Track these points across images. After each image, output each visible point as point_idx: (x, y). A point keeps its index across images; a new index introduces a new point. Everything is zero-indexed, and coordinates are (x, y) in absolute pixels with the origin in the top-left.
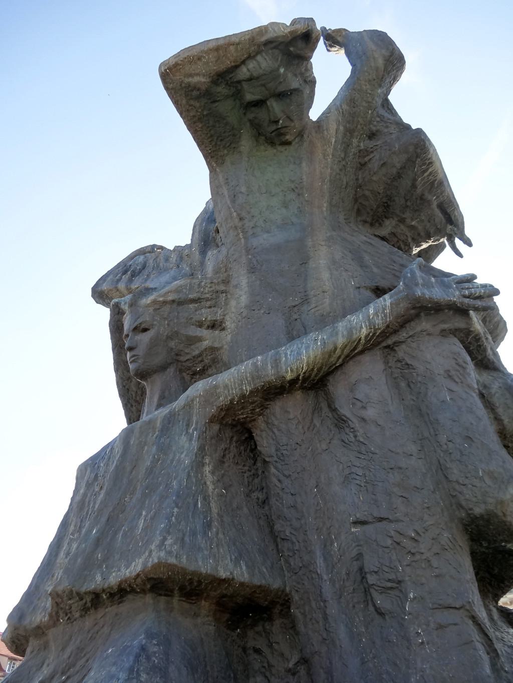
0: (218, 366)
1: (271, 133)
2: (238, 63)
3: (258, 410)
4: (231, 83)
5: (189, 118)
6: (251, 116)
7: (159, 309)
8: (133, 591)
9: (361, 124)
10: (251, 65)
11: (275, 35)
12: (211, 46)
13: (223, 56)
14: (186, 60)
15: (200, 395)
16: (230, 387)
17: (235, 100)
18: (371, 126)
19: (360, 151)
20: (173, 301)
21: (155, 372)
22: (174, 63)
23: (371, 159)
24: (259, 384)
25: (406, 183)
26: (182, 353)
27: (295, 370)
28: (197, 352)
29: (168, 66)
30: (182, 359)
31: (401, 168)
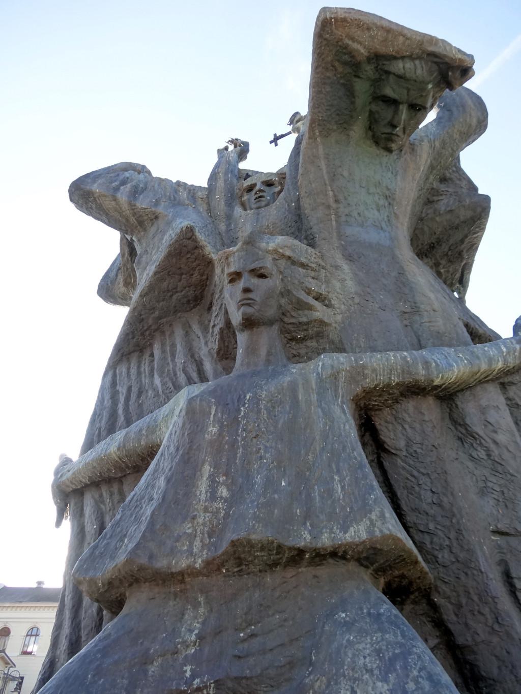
0: (321, 341)
1: (382, 134)
2: (398, 56)
3: (390, 402)
4: (380, 69)
5: (322, 76)
6: (374, 107)
7: (277, 260)
8: (344, 557)
9: (441, 166)
10: (409, 65)
11: (445, 53)
12: (385, 24)
13: (391, 41)
14: (356, 22)
15: (346, 369)
16: (378, 372)
17: (371, 85)
18: (446, 172)
19: (432, 189)
20: (289, 258)
21: (264, 324)
22: (342, 16)
23: (439, 200)
24: (408, 379)
25: (458, 236)
26: (288, 314)
27: (445, 378)
28: (304, 320)
29: (336, 15)
30: (286, 319)
31: (462, 222)
